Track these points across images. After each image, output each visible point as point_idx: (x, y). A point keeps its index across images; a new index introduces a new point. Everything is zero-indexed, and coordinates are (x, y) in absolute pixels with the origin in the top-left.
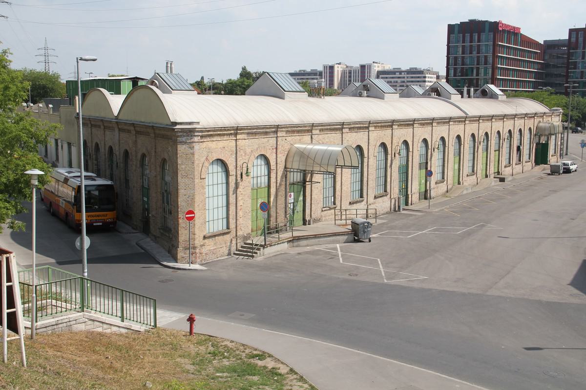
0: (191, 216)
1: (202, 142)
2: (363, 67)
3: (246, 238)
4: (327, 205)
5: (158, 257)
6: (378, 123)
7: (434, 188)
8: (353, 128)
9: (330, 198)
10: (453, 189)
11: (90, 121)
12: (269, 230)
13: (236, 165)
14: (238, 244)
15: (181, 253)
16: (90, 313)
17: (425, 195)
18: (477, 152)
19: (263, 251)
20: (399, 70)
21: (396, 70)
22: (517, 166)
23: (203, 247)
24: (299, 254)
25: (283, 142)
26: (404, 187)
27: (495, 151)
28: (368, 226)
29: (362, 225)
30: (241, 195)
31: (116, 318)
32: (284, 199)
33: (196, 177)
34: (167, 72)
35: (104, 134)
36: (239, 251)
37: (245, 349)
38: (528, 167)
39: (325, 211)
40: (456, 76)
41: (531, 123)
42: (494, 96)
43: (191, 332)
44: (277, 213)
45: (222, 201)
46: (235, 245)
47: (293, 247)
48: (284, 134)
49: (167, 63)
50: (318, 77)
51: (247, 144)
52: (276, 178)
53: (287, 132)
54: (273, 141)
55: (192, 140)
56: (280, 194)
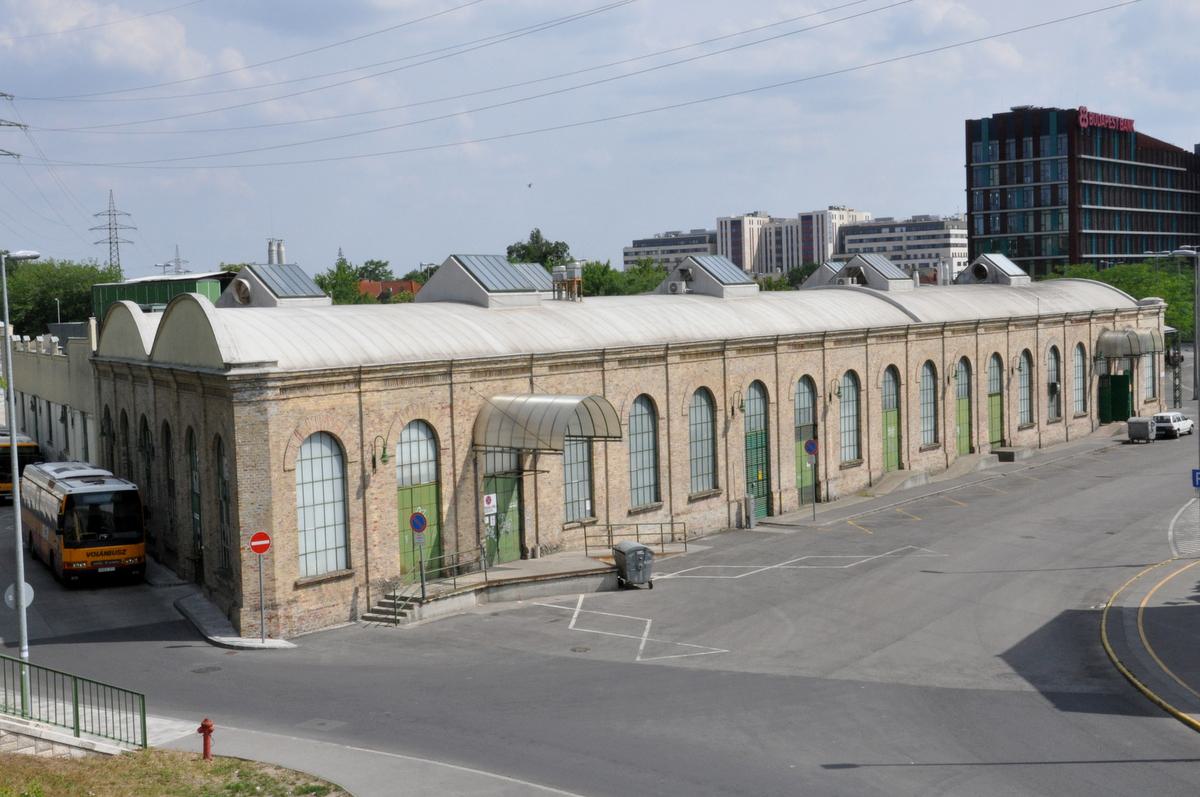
0: (263, 544)
1: (284, 399)
2: (806, 219)
3: (387, 586)
4: (576, 518)
5: (206, 628)
6: (688, 347)
7: (836, 479)
8: (630, 359)
9: (582, 503)
10: (884, 479)
11: (111, 366)
12: (441, 569)
13: (362, 442)
14: (371, 599)
15: (246, 618)
16: (28, 724)
17: (813, 493)
18: (943, 398)
19: (419, 612)
20: (889, 223)
21: (882, 223)
22: (1051, 427)
23: (294, 605)
24: (495, 614)
25: (466, 393)
26: (760, 477)
27: (990, 396)
28: (644, 556)
29: (631, 556)
30: (374, 501)
31: (65, 729)
32: (472, 506)
33: (274, 468)
34: (270, 261)
35: (134, 391)
36: (374, 611)
37: (298, 779)
38: (1081, 425)
39: (570, 529)
40: (989, 233)
41: (1089, 334)
42: (999, 279)
43: (206, 754)
44: (457, 535)
45: (333, 514)
46: (365, 600)
47: (489, 601)
48: (467, 377)
49: (270, 244)
50: (708, 246)
51: (385, 399)
52: (454, 465)
53: (474, 373)
54: (442, 393)
55: (263, 397)
56: (462, 496)
